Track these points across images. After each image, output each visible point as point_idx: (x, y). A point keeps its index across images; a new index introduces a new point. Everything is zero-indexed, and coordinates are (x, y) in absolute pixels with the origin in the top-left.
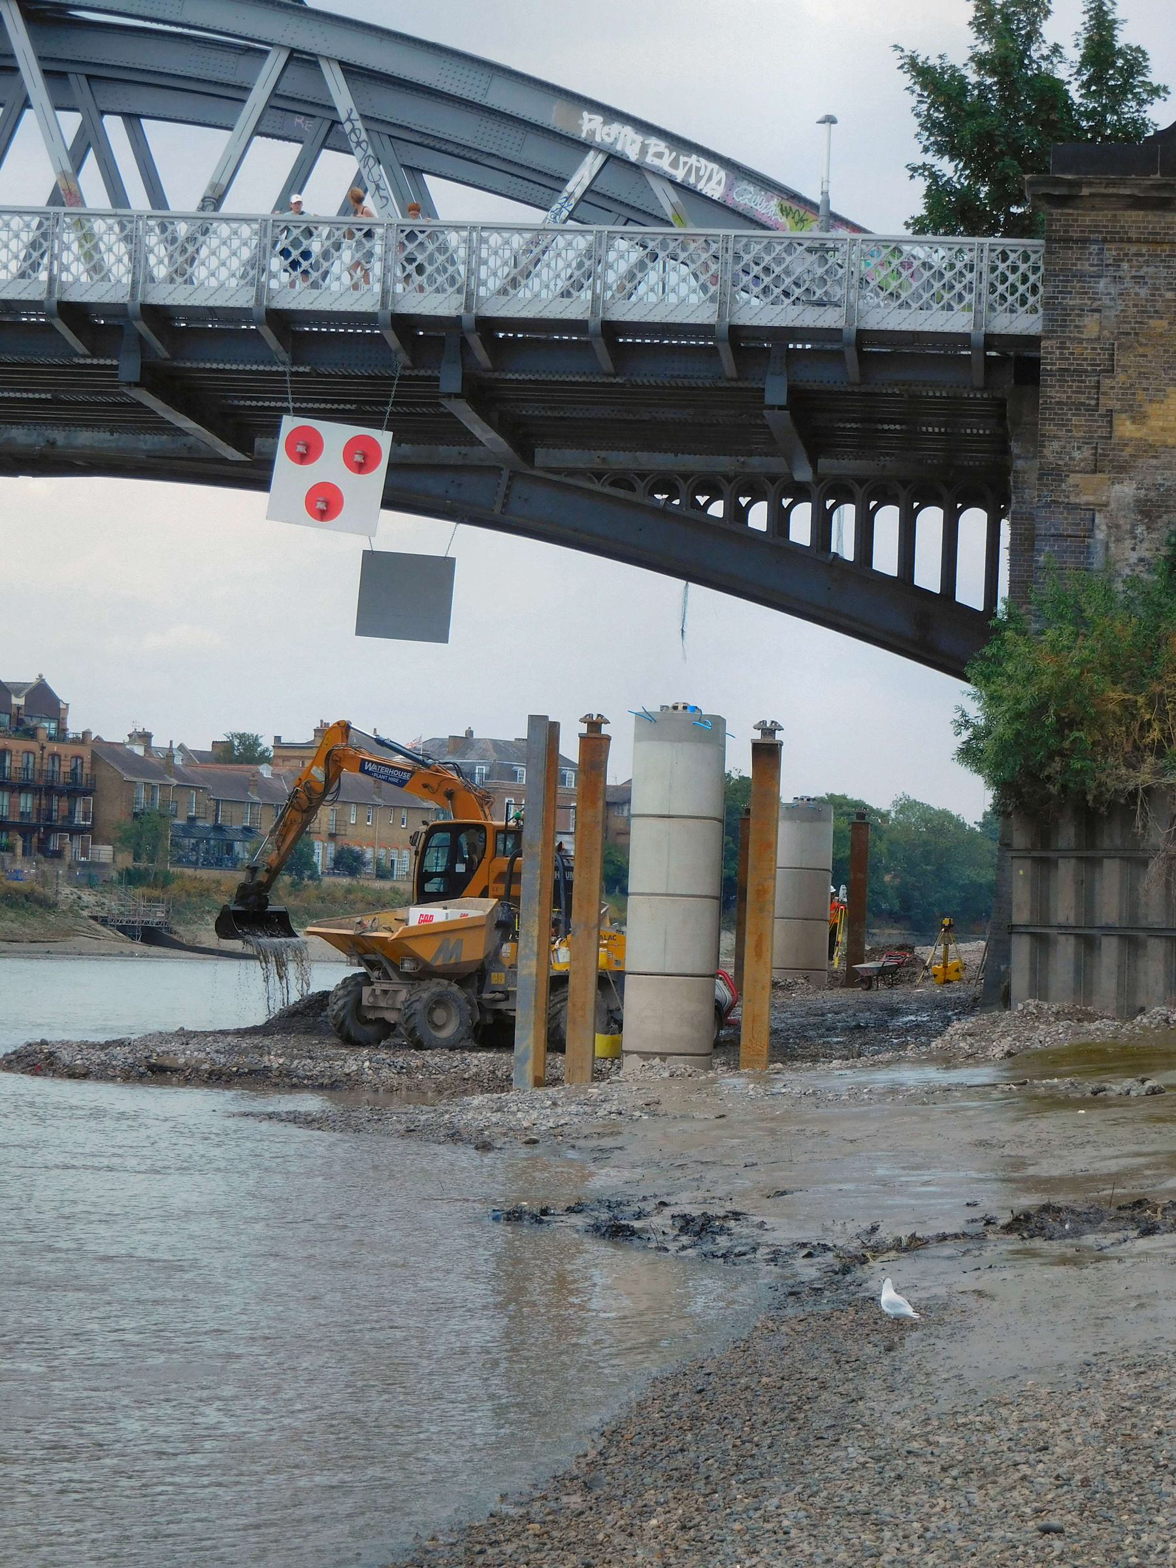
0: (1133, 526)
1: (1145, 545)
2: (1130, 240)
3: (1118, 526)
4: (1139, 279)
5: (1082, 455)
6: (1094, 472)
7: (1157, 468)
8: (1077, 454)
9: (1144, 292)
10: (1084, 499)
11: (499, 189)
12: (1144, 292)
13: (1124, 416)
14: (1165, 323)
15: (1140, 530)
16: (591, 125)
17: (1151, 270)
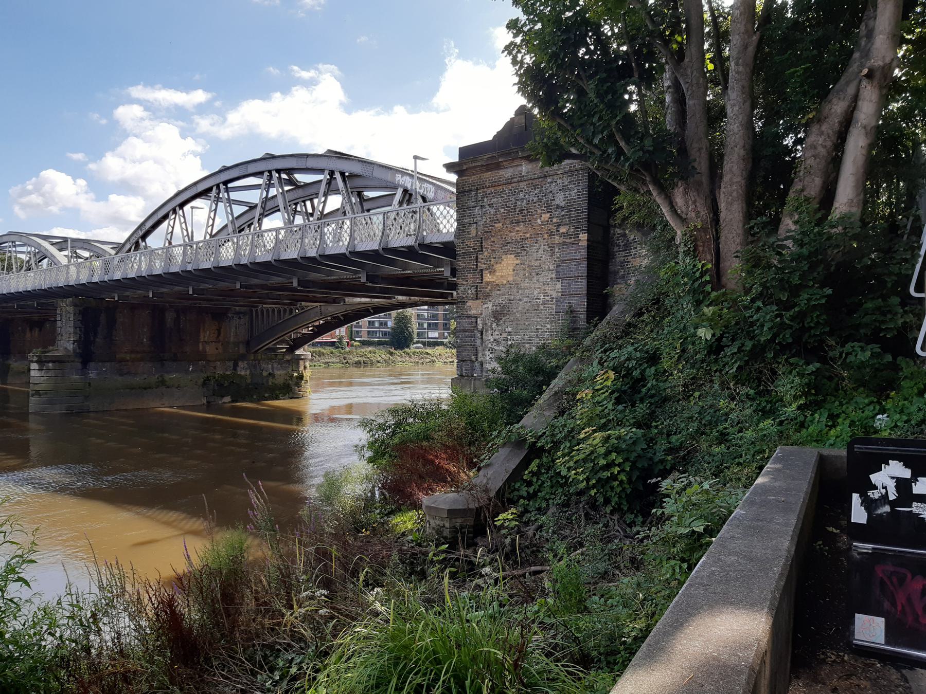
0: (492, 324)
1: (496, 333)
2: (486, 187)
3: (486, 324)
4: (491, 205)
5: (471, 292)
6: (477, 299)
7: (499, 295)
8: (469, 292)
9: (493, 211)
10: (473, 312)
11: (382, 205)
12: (493, 211)
13: (487, 272)
14: (500, 225)
15: (494, 325)
16: (399, 178)
17: (495, 200)
